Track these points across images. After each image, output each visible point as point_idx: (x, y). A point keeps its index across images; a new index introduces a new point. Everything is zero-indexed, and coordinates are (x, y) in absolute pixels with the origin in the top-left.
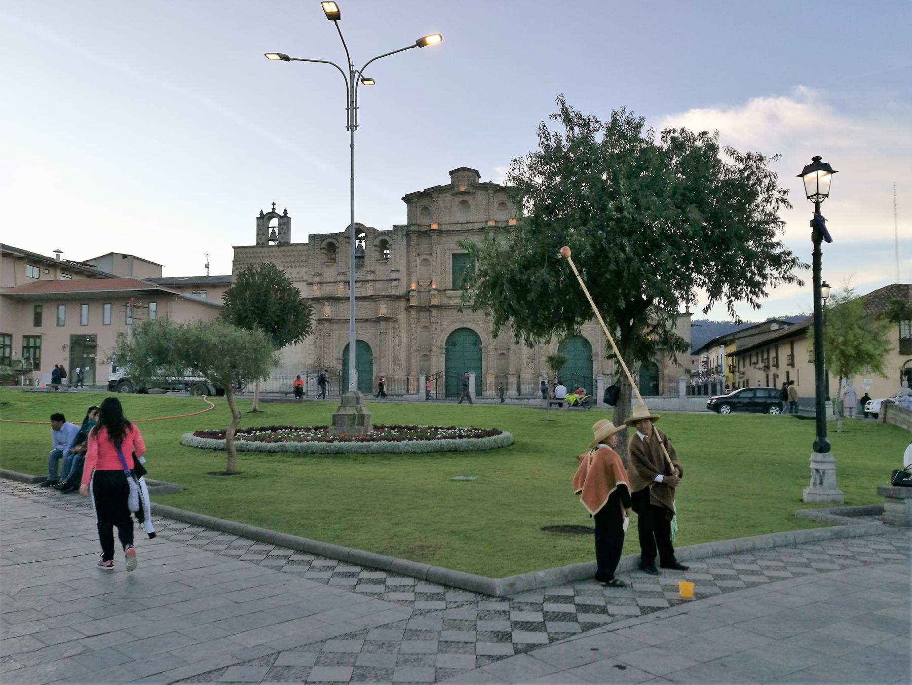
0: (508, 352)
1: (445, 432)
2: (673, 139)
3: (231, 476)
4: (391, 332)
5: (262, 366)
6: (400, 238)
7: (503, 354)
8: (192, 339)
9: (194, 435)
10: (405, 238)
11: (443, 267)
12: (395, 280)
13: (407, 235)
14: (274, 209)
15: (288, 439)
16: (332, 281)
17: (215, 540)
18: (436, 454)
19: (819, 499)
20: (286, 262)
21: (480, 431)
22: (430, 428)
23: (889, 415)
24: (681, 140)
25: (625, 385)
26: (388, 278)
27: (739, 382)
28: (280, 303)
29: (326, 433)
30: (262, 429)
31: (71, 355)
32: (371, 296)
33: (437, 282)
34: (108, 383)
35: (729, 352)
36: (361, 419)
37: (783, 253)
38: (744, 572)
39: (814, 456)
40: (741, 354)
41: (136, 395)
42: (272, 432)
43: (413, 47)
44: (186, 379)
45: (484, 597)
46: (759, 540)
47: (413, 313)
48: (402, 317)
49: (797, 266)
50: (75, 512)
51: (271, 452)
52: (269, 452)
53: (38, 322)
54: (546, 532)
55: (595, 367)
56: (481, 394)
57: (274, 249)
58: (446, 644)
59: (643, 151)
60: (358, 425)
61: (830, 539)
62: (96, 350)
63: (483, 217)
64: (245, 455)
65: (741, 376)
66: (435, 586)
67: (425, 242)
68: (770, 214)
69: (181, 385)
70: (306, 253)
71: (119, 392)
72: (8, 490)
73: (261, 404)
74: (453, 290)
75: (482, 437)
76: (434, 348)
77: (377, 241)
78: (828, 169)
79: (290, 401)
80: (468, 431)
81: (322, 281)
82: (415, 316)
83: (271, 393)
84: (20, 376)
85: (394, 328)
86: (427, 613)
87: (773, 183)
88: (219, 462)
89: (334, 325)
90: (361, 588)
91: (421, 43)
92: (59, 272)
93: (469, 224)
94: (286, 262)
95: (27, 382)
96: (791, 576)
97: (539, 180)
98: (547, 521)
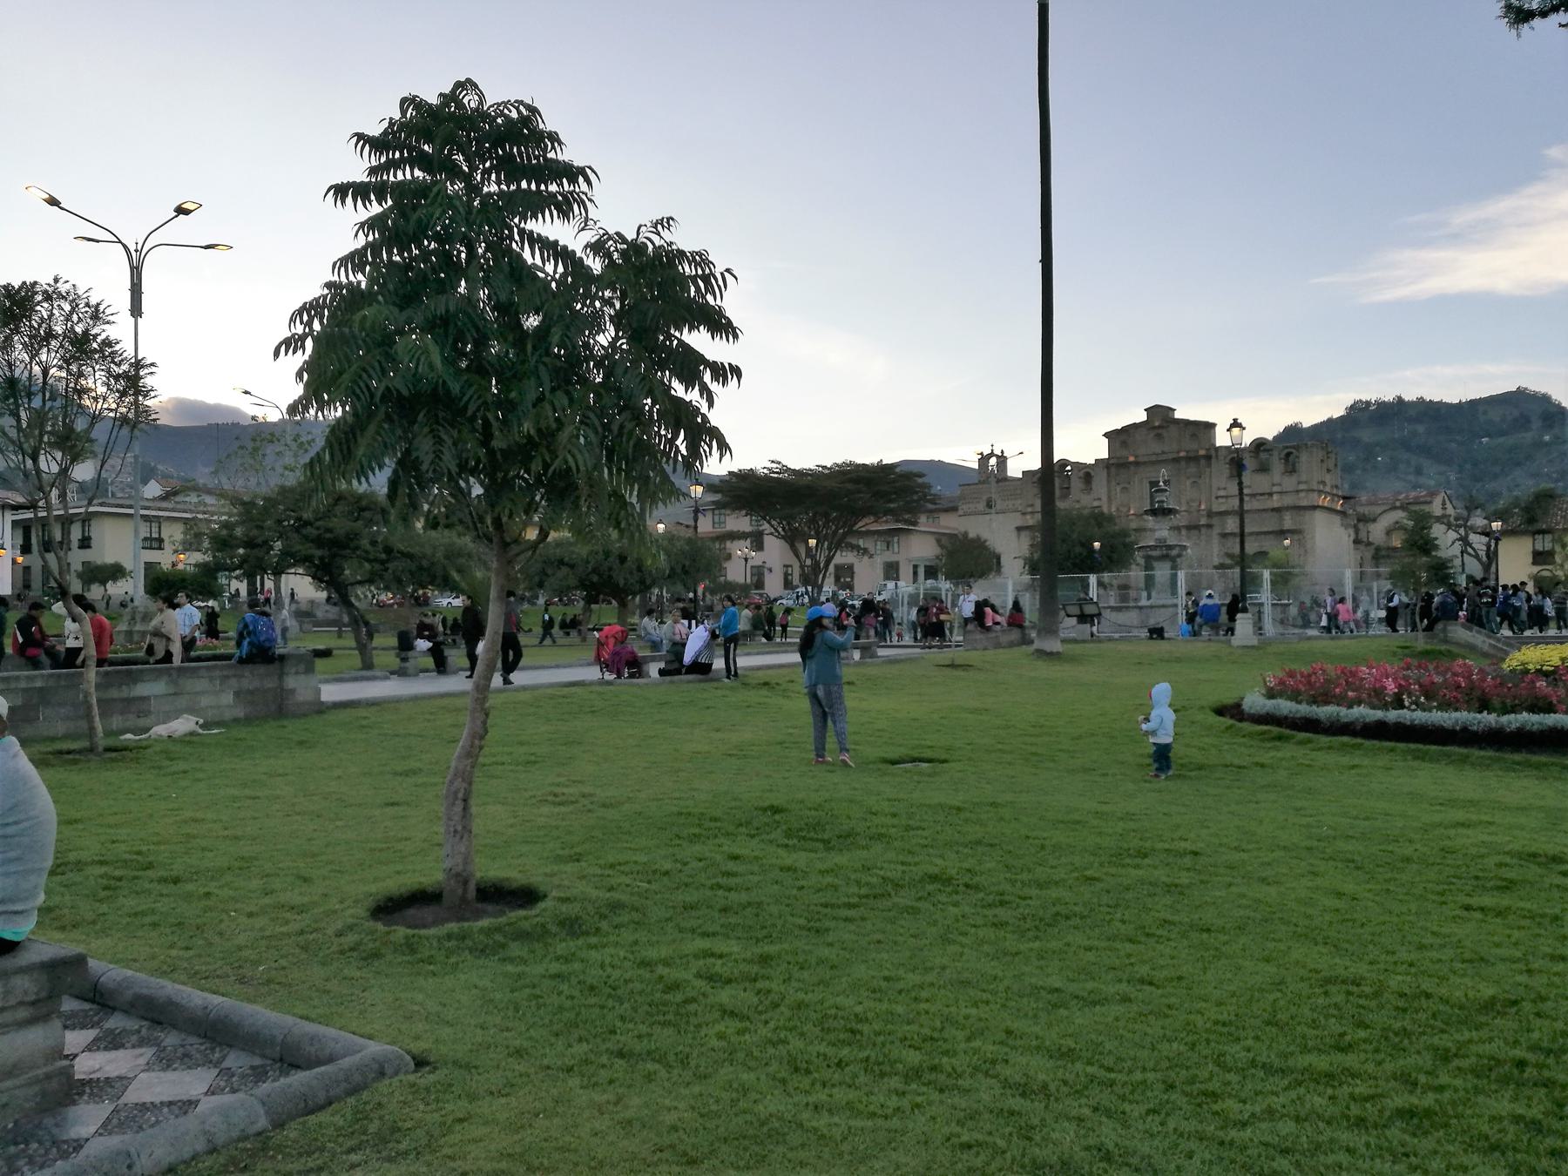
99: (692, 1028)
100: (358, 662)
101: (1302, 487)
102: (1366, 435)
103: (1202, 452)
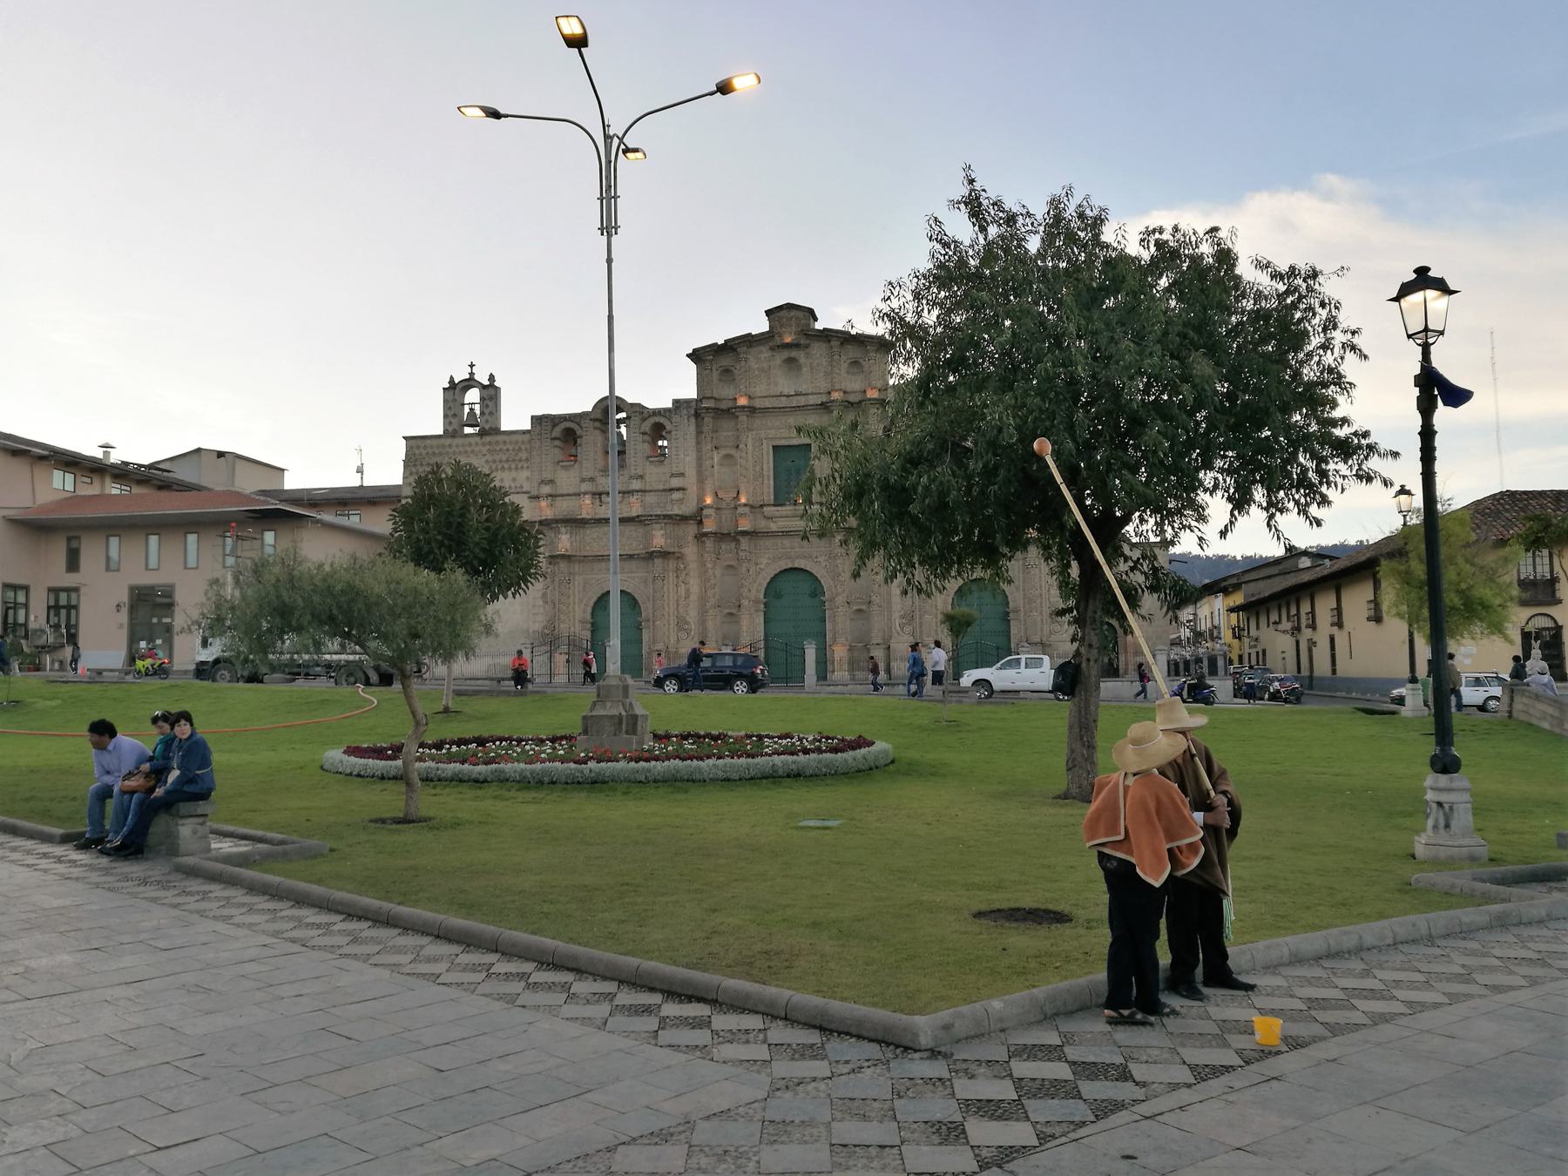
0: (869, 607)
1: (776, 743)
2: (1160, 245)
3: (411, 825)
4: (671, 576)
5: (463, 633)
6: (686, 421)
7: (860, 611)
8: (338, 587)
9: (345, 752)
10: (693, 420)
11: (758, 468)
12: (678, 489)
13: (697, 415)
14: (472, 374)
15: (509, 759)
16: (571, 492)
17: (391, 944)
18: (765, 781)
19: (1443, 853)
20: (494, 461)
21: (835, 741)
22: (749, 737)
23: (1518, 706)
24: (1172, 244)
25: (1088, 660)
26: (667, 487)
27: (1250, 654)
28: (487, 529)
29: (571, 747)
30: (460, 742)
31: (131, 618)
32: (638, 516)
33: (747, 492)
34: (194, 667)
35: (1232, 604)
36: (632, 723)
37: (1355, 434)
38: (1356, 992)
39: (1431, 779)
40: (1252, 608)
41: (241, 685)
42: (478, 746)
43: (712, 94)
44: (327, 657)
45: (898, 1051)
46: (1370, 932)
47: (709, 544)
48: (690, 551)
49: (1376, 455)
50: (134, 895)
51: (479, 782)
52: (477, 781)
53: (73, 564)
54: (984, 921)
55: (1014, 631)
56: (825, 678)
57: (472, 440)
58: (845, 1150)
59: (1108, 262)
60: (627, 733)
61: (1489, 928)
62: (173, 612)
63: (823, 385)
64: (434, 787)
65: (1252, 643)
66: (802, 1031)
67: (727, 424)
68: (1331, 370)
69: (319, 669)
70: (528, 447)
71: (214, 680)
72: (16, 856)
73: (458, 699)
74: (774, 505)
75: (842, 751)
76: (745, 602)
77: (647, 426)
78: (1442, 286)
79: (507, 693)
80: (815, 740)
81: (554, 493)
82: (712, 549)
83: (470, 679)
84: (44, 655)
85: (677, 569)
86: (799, 1084)
87: (1335, 317)
88: (390, 800)
89: (577, 566)
90: (666, 1036)
91: (724, 88)
92: (108, 480)
93: (799, 397)
94: (501, 461)
95: (56, 666)
96: (1446, 1000)
97: (931, 317)
98: (982, 902)
99: (901, 989)
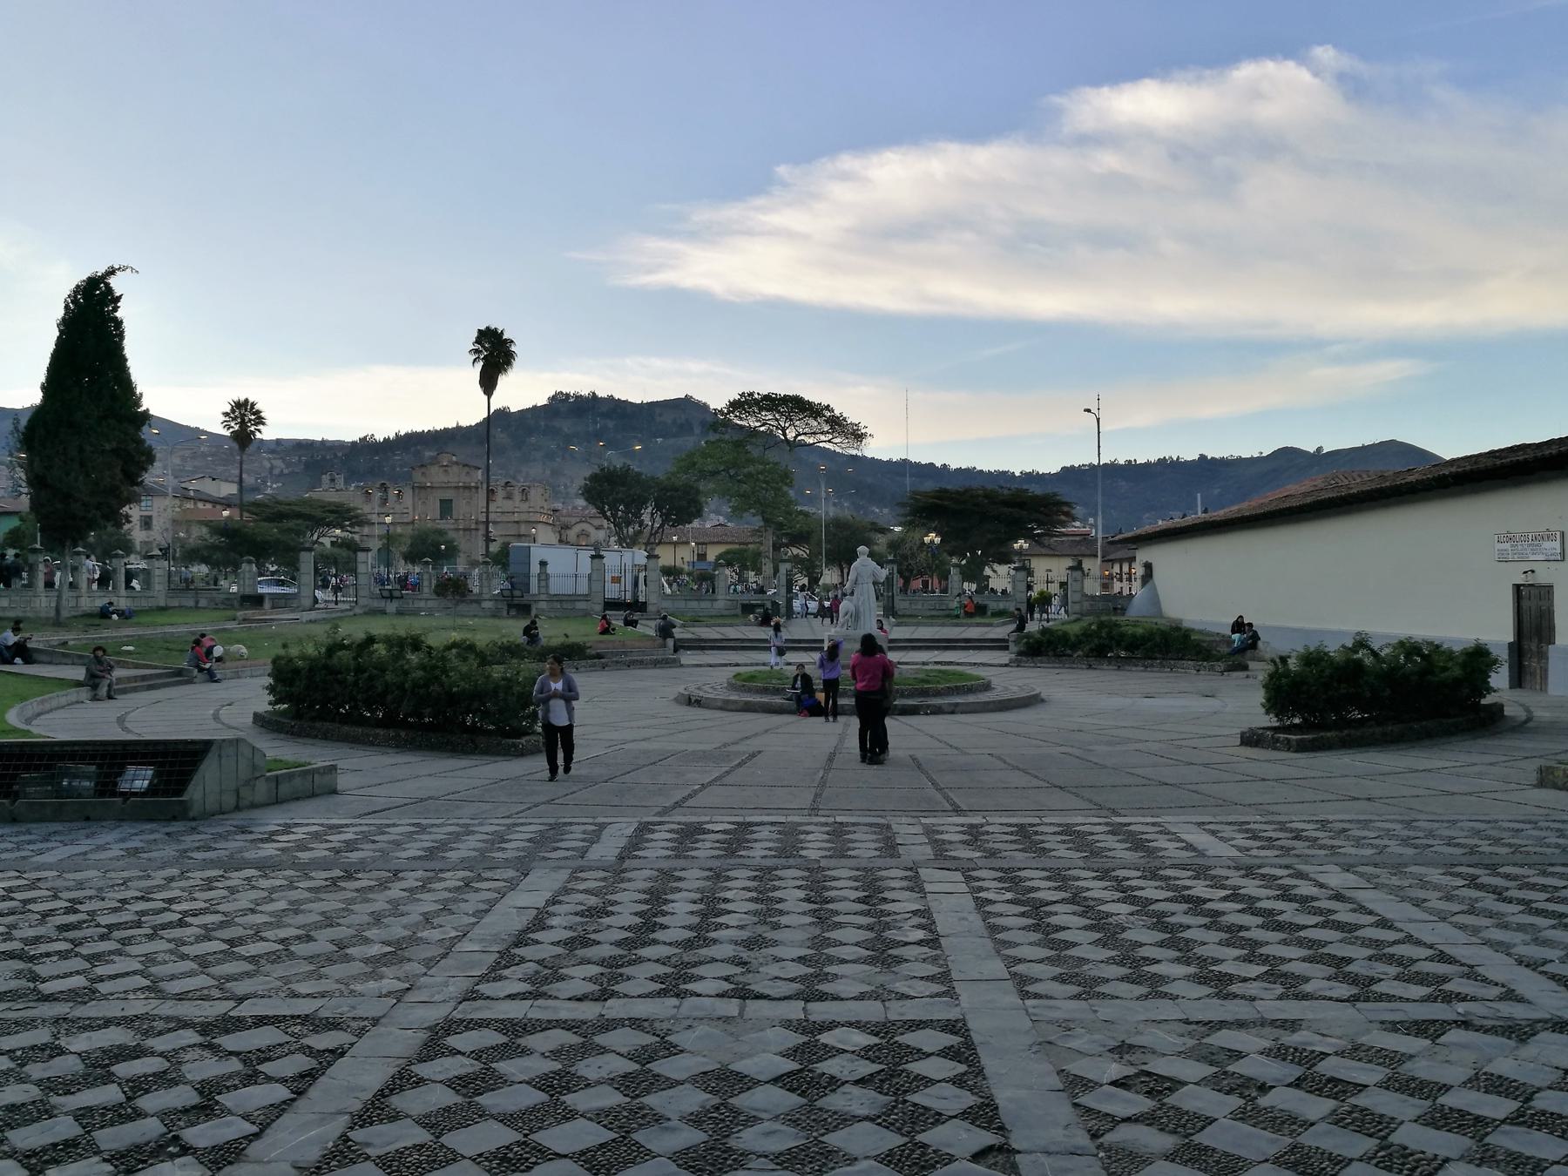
63: (456, 479)
100: (547, 774)
101: (531, 510)
102: (566, 426)
103: (473, 484)
